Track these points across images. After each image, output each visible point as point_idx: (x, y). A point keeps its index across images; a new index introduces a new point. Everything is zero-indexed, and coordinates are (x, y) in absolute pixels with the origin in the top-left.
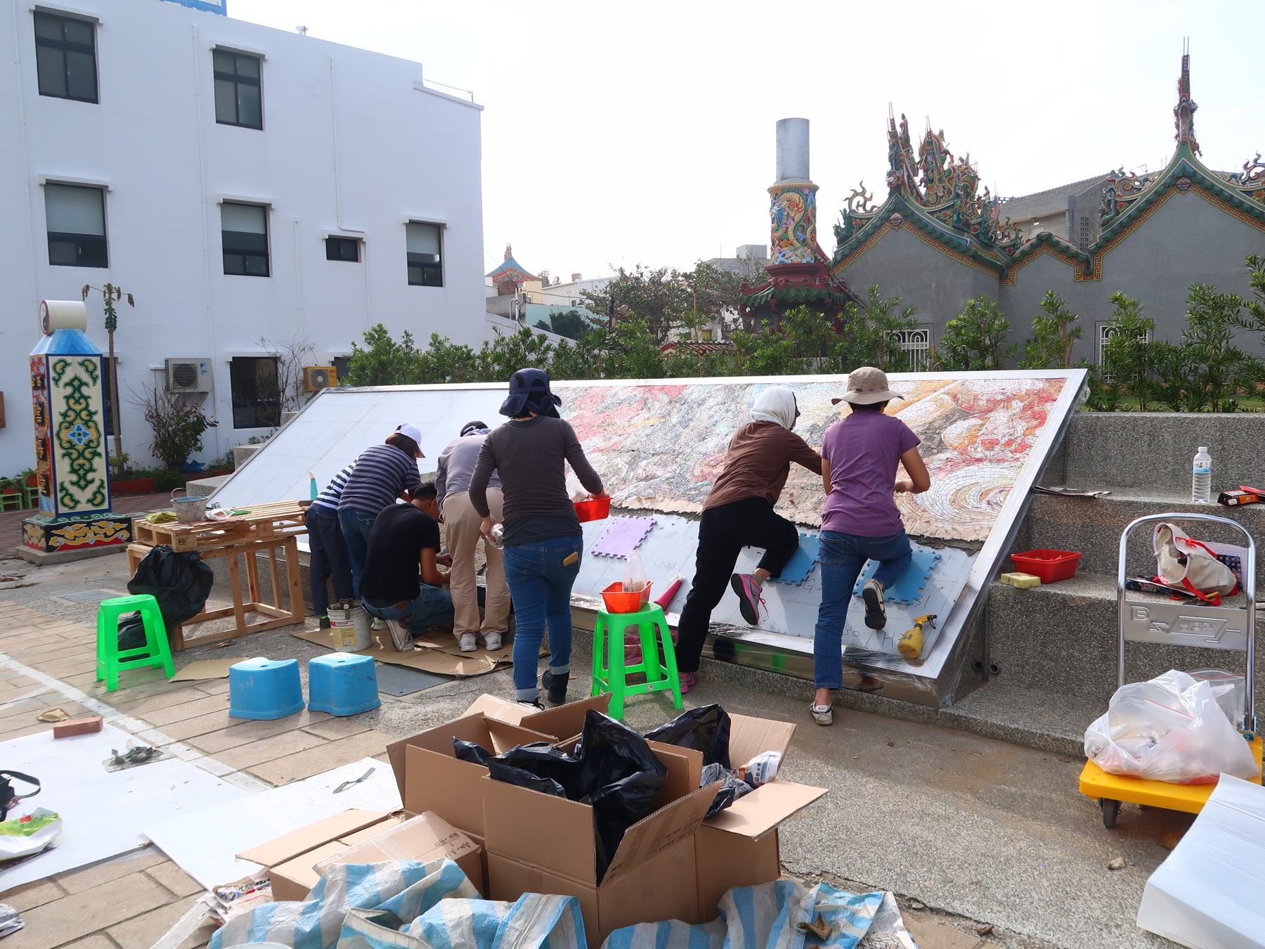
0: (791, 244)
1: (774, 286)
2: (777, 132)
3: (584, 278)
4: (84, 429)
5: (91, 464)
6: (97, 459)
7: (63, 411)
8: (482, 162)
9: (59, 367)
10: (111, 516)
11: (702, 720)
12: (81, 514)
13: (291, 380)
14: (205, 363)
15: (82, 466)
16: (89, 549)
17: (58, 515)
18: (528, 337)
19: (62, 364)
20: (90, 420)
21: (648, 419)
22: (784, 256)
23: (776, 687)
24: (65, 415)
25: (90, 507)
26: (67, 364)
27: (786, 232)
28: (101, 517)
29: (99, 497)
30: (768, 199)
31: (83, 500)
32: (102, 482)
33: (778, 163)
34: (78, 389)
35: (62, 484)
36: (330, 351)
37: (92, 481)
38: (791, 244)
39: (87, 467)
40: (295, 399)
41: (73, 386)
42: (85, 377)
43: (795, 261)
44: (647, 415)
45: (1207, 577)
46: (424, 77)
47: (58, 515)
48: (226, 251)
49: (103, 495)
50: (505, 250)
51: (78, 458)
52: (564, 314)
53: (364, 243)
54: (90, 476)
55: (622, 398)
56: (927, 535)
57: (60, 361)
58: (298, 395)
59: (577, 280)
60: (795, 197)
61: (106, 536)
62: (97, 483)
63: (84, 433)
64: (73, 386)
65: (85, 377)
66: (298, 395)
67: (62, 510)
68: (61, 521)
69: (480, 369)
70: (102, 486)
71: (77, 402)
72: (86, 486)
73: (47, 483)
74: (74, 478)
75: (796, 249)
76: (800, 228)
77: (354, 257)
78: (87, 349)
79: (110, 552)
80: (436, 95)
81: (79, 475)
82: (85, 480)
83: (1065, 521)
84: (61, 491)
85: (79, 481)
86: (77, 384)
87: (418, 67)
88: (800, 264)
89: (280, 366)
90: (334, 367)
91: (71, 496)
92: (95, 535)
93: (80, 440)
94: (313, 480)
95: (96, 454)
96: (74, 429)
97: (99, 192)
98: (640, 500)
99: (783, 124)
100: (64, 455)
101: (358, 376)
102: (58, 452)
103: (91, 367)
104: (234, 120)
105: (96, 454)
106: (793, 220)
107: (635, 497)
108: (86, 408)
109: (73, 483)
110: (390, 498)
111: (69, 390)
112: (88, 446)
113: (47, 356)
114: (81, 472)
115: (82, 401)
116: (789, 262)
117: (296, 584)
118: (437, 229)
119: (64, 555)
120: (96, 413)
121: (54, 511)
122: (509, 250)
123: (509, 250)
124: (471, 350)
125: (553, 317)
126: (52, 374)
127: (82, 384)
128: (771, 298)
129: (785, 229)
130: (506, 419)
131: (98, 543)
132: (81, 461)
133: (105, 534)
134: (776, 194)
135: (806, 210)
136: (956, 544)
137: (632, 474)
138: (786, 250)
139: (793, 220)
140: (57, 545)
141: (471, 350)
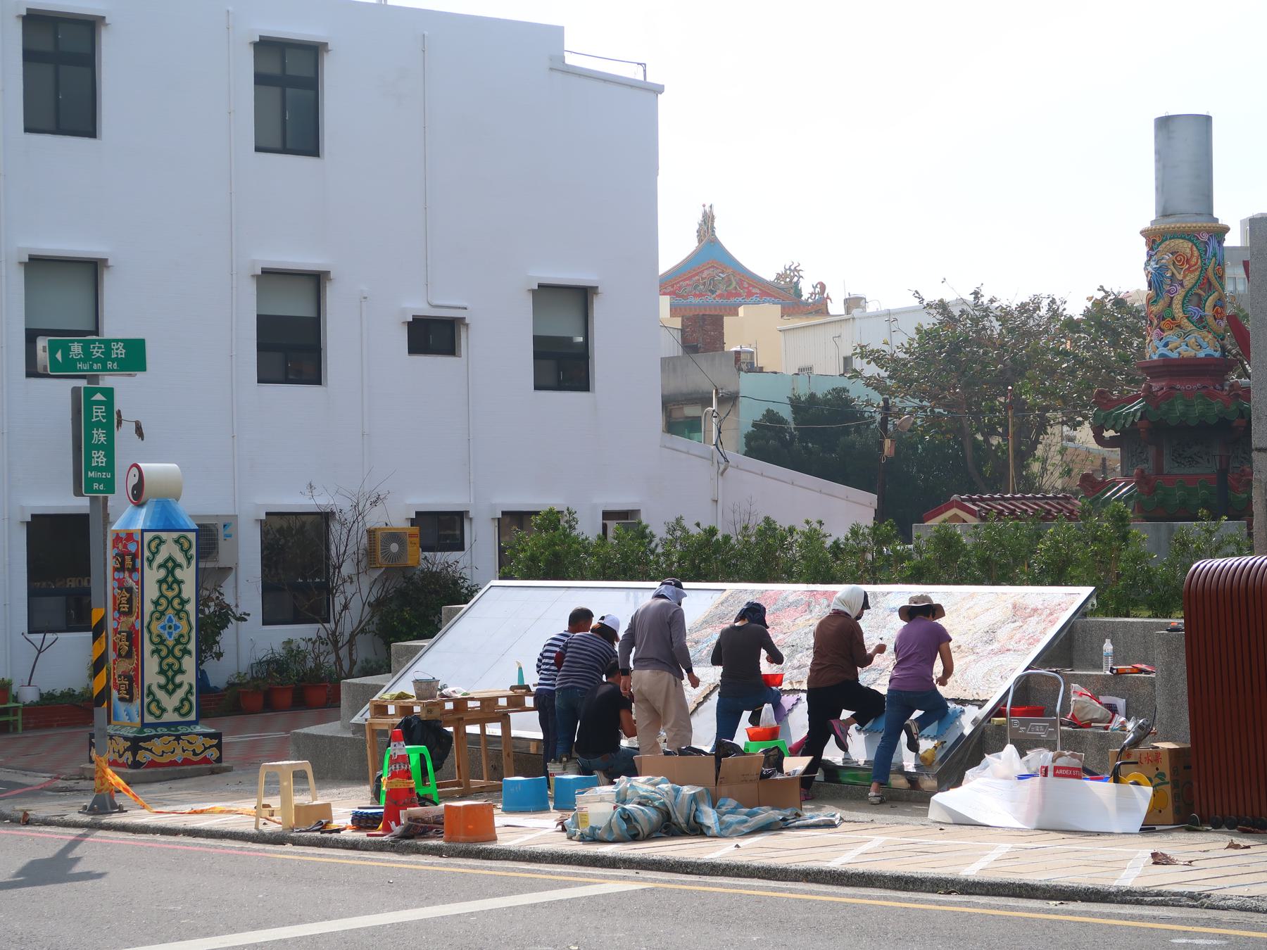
0: (1179, 326)
1: (1144, 397)
2: (1156, 137)
3: (871, 308)
4: (175, 620)
5: (180, 664)
6: (187, 657)
7: (154, 598)
8: (659, 178)
9: (153, 545)
10: (198, 729)
11: (771, 753)
12: (168, 725)
13: (352, 548)
14: (229, 523)
15: (170, 666)
16: (178, 768)
17: (144, 725)
18: (713, 536)
19: (157, 541)
20: (182, 610)
21: (809, 620)
22: (1166, 345)
23: (859, 794)
24: (156, 603)
25: (176, 718)
26: (162, 542)
27: (1170, 305)
28: (189, 730)
29: (186, 703)
30: (1140, 248)
31: (170, 708)
32: (191, 685)
33: (1157, 189)
34: (171, 572)
35: (149, 687)
36: (409, 501)
37: (180, 685)
38: (1179, 326)
39: (176, 667)
40: (355, 579)
41: (167, 568)
42: (180, 558)
43: (1185, 354)
44: (808, 617)
45: (1086, 713)
46: (568, 45)
47: (144, 725)
48: (261, 348)
49: (191, 704)
50: (700, 218)
51: (167, 657)
52: (819, 395)
53: (467, 325)
54: (178, 679)
55: (791, 601)
56: (961, 698)
57: (155, 538)
58: (359, 573)
59: (856, 312)
60: (1185, 246)
61: (195, 754)
62: (185, 688)
63: (175, 625)
64: (167, 568)
65: (180, 558)
66: (359, 573)
67: (149, 719)
68: (148, 732)
69: (664, 566)
70: (189, 692)
71: (170, 588)
72: (174, 690)
73: (131, 685)
74: (162, 680)
75: (1187, 334)
76: (1195, 299)
77: (450, 348)
78: (182, 523)
79: (199, 774)
80: (580, 75)
81: (167, 677)
82: (173, 683)
83: (1045, 688)
84: (148, 696)
85: (167, 684)
86: (170, 566)
87: (555, 34)
88: (1195, 358)
89: (335, 528)
90: (416, 530)
91: (158, 702)
92: (184, 751)
93: (170, 634)
94: (520, 669)
95: (186, 652)
96: (165, 621)
97: (93, 269)
98: (791, 683)
99: (1165, 124)
100: (153, 652)
101: (528, 568)
102: (148, 647)
103: (186, 545)
104: (278, 145)
105: (186, 652)
106: (1182, 285)
107: (789, 681)
108: (179, 595)
109: (161, 687)
110: (597, 676)
111: (162, 573)
112: (178, 642)
113: (143, 531)
114: (170, 673)
115: (175, 586)
116: (1174, 355)
117: (508, 755)
118: (583, 296)
119: (152, 772)
120: (188, 601)
121: (138, 720)
122: (708, 221)
123: (708, 221)
124: (646, 527)
125: (796, 404)
126: (147, 554)
127: (178, 565)
128: (1141, 419)
129: (1167, 300)
130: (720, 669)
131: (186, 762)
132: (170, 660)
133: (194, 751)
134: (1154, 241)
135: (1204, 269)
136: (975, 703)
137: (789, 664)
138: (1169, 335)
139: (1182, 285)
140: (144, 760)
141: (646, 527)
